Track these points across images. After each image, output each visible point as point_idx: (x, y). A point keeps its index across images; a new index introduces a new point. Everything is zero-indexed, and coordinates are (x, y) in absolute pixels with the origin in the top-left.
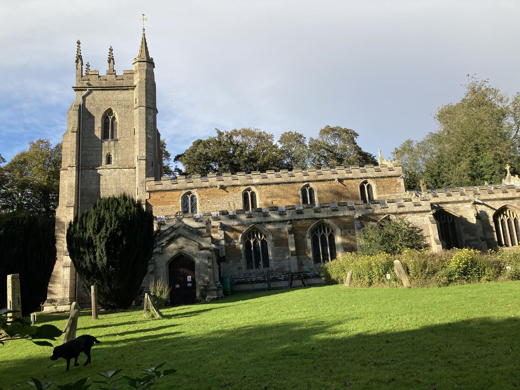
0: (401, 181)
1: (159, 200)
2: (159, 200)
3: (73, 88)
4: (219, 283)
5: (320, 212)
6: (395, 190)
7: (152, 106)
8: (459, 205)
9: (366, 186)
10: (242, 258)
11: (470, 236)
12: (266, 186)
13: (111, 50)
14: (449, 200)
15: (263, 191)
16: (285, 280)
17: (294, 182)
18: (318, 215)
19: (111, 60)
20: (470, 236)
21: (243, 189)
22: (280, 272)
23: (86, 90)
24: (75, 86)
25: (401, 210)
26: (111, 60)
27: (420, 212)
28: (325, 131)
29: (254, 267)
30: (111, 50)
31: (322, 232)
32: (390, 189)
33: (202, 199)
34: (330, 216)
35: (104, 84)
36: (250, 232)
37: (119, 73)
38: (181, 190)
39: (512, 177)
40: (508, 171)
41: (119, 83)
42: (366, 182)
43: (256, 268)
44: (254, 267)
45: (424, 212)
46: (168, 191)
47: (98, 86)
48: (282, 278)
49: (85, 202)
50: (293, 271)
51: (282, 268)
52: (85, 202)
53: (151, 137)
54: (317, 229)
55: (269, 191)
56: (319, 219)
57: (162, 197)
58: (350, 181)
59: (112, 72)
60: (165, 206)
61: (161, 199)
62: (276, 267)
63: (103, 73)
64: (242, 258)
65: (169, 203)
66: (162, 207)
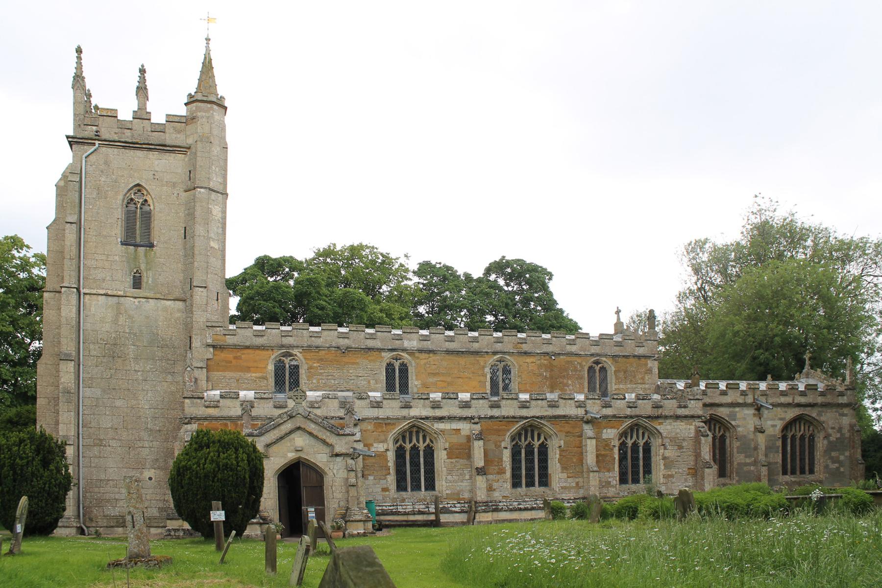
0: (654, 365)
1: (231, 362)
2: (231, 362)
3: (68, 137)
4: (365, 511)
5: (499, 407)
6: (643, 378)
7: (220, 188)
8: (737, 409)
9: (597, 368)
10: (389, 474)
11: (746, 457)
12: (427, 355)
13: (142, 71)
14: (724, 401)
15: (423, 362)
16: (462, 512)
17: (476, 353)
18: (524, 412)
19: (142, 90)
20: (746, 457)
21: (387, 356)
22: (454, 499)
23: (94, 144)
24: (71, 133)
25: (657, 412)
26: (142, 90)
27: (686, 417)
28: (498, 267)
29: (409, 489)
30: (142, 71)
31: (529, 439)
32: (635, 377)
33: (310, 368)
34: (545, 414)
35: (127, 136)
36: (405, 431)
37: (158, 117)
38: (272, 348)
39: (812, 371)
40: (807, 362)
41: (156, 138)
42: (597, 363)
43: (426, 489)
44: (409, 489)
45: (693, 417)
46: (247, 347)
47: (117, 139)
48: (457, 509)
49: (92, 354)
50: (479, 499)
51: (458, 494)
52: (92, 354)
53: (216, 247)
54: (520, 434)
55: (432, 363)
56: (527, 418)
57: (236, 358)
58: (574, 358)
59: (142, 115)
60: (242, 374)
61: (234, 362)
62: (447, 492)
63: (126, 114)
64: (389, 474)
65: (248, 369)
66: (237, 375)
